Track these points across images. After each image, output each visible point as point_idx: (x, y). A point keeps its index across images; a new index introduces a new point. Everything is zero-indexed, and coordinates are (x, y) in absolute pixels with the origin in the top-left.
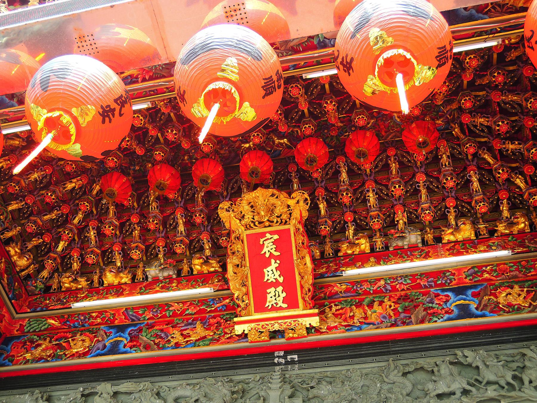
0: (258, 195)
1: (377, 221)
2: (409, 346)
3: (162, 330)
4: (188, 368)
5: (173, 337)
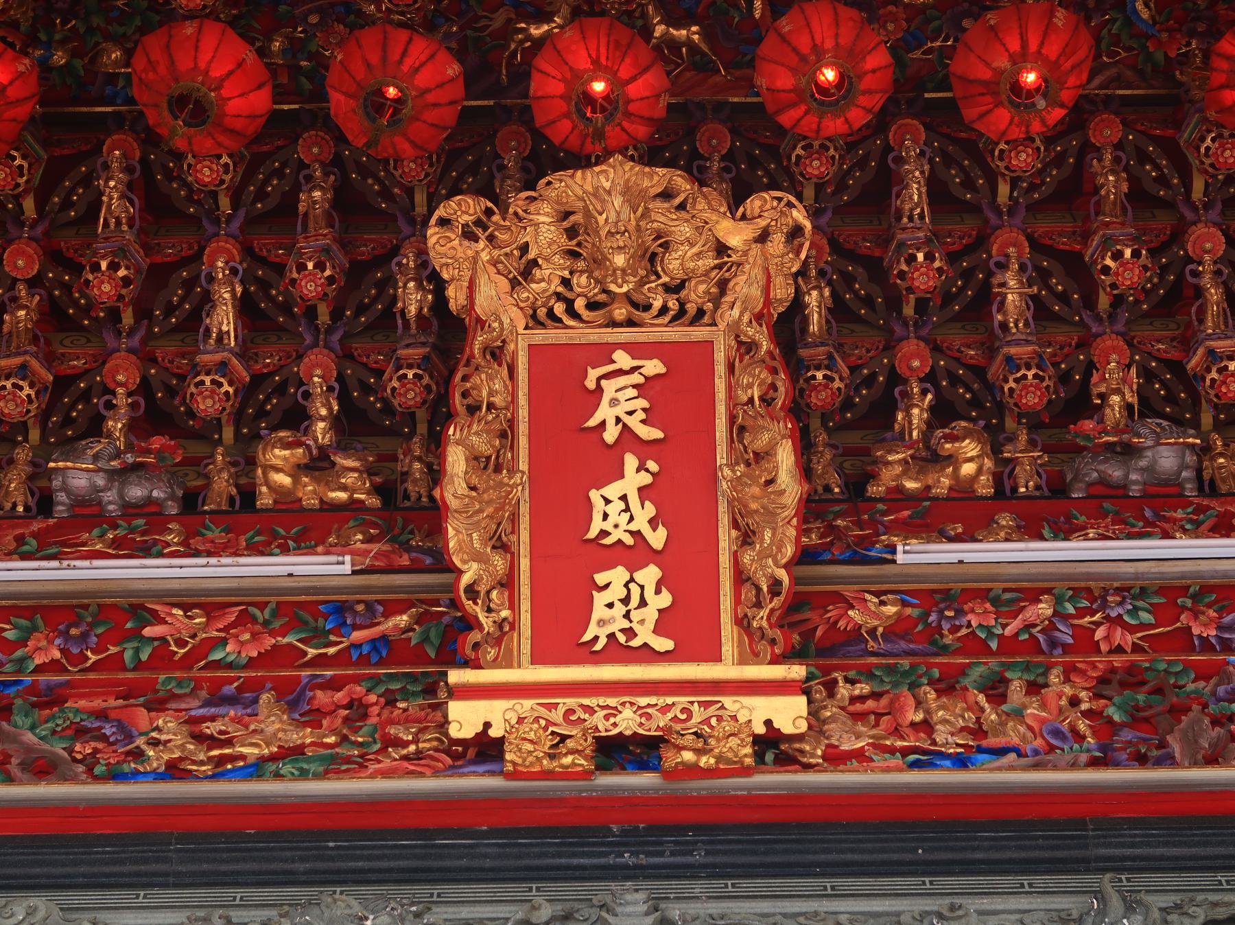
0: (607, 185)
1: (1035, 376)
2: (1166, 844)
3: (102, 715)
4: (223, 861)
5: (155, 743)
